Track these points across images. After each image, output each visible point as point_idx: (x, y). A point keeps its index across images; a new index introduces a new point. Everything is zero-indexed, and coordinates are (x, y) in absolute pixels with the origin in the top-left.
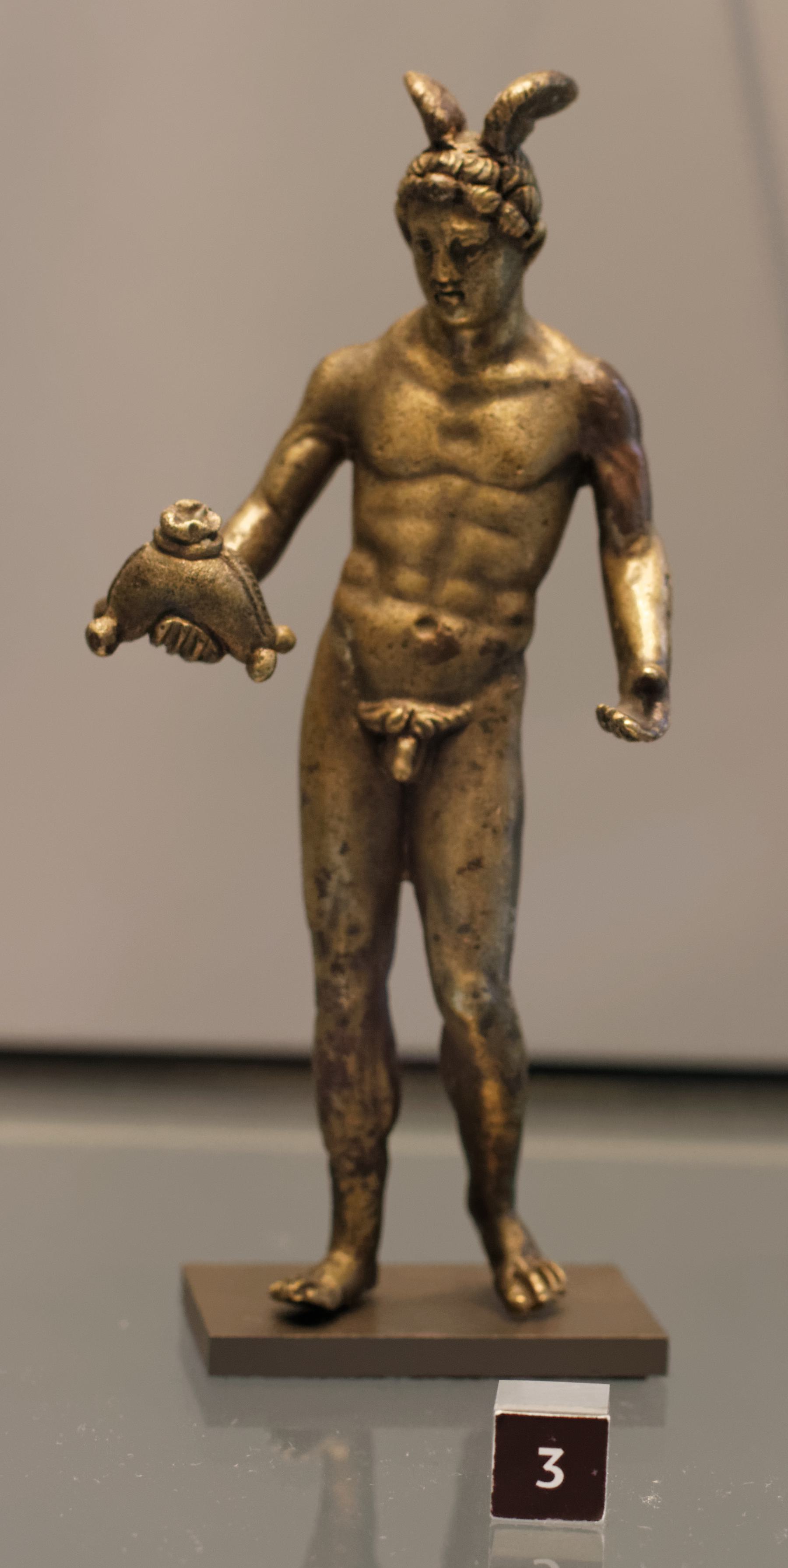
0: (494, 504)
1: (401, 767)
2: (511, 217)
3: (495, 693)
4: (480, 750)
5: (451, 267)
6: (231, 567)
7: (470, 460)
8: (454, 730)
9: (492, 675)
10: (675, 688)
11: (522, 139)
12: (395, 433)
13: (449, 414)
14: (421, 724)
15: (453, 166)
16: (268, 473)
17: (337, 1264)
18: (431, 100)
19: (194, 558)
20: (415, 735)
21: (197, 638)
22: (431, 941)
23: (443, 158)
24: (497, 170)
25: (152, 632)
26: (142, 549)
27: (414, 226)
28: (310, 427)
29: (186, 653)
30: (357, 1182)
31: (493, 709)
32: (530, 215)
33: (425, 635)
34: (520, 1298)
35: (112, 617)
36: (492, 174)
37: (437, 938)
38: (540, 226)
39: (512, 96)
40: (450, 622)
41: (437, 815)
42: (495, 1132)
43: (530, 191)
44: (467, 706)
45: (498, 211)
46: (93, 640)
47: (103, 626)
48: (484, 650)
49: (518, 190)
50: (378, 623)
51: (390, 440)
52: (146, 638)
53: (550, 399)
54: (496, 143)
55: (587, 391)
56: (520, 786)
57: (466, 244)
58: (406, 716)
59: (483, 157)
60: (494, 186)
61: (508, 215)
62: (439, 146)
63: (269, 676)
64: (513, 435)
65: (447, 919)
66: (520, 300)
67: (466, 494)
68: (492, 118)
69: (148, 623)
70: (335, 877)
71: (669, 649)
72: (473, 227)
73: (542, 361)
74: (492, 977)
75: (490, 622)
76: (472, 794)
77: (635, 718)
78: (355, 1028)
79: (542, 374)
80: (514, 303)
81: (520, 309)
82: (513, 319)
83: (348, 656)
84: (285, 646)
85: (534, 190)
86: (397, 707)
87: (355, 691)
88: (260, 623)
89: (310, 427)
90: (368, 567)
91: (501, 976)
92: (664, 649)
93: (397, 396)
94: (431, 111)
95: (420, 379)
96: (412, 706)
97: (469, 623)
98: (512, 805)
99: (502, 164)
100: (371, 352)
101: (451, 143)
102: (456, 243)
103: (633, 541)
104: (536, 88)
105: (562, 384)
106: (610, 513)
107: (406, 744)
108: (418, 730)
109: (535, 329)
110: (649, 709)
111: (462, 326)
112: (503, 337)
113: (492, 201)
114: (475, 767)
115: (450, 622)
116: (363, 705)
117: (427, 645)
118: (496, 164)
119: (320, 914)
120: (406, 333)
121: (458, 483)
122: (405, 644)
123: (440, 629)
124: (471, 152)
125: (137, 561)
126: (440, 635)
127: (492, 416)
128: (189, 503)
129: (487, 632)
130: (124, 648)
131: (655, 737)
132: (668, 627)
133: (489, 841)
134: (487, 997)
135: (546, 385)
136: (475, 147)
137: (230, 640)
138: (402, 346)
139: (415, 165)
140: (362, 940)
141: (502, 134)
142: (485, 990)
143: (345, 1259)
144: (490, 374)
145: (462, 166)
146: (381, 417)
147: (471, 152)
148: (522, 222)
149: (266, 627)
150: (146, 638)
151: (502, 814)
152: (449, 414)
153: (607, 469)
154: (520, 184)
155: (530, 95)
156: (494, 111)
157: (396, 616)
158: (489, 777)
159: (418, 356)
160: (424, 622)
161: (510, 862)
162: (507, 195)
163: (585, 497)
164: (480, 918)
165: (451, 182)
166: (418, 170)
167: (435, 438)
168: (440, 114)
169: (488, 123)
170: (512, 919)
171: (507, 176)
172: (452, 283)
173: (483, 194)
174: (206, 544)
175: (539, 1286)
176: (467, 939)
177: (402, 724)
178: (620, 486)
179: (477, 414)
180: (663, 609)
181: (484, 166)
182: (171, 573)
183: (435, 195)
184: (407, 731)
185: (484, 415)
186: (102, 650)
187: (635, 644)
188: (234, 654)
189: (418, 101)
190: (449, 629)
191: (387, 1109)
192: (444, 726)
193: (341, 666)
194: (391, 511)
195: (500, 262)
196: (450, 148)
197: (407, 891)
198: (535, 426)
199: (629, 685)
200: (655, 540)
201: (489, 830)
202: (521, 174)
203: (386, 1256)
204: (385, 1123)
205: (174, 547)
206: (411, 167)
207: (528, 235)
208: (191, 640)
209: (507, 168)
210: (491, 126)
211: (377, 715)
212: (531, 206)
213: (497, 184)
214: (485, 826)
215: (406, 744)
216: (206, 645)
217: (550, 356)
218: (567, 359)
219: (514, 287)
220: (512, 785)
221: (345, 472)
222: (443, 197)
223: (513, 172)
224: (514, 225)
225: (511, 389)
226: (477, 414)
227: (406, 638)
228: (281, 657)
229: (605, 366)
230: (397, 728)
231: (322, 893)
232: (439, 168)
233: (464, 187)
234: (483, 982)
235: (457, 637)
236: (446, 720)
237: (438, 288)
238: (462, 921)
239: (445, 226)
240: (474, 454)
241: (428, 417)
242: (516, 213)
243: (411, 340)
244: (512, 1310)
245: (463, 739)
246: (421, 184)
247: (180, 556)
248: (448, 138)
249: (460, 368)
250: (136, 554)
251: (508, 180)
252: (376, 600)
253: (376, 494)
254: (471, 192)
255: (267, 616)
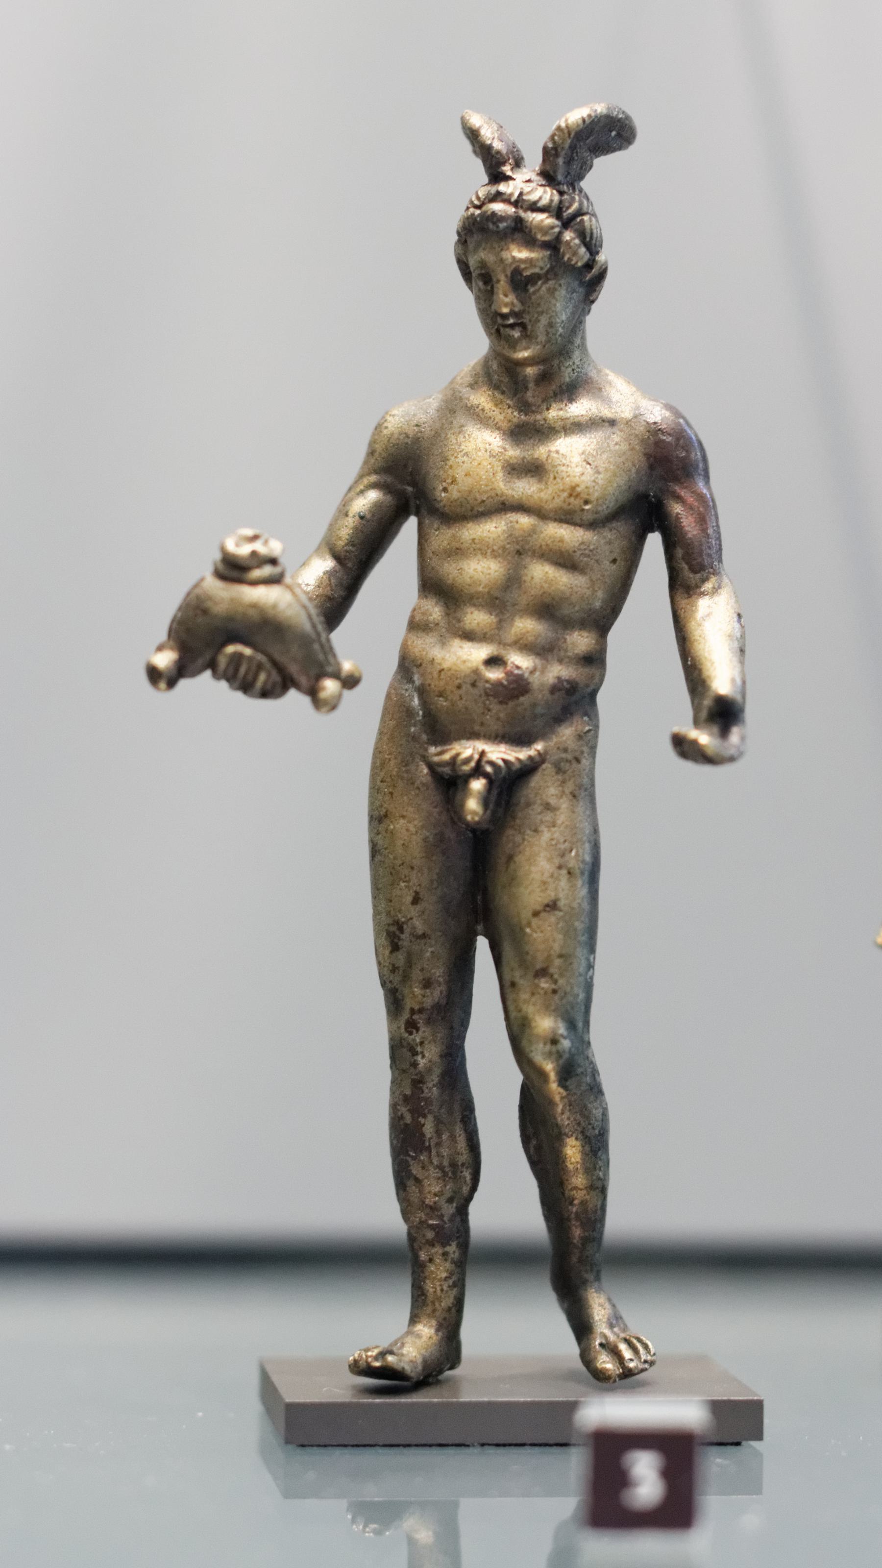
0: (561, 540)
1: (473, 805)
2: (572, 244)
3: (567, 733)
4: (552, 790)
5: (511, 298)
6: (293, 593)
7: (536, 497)
8: (528, 770)
9: (563, 715)
10: (750, 713)
11: (581, 177)
12: (459, 474)
13: (514, 453)
14: (492, 763)
15: (511, 195)
16: (332, 527)
17: (419, 1336)
18: (488, 134)
19: (254, 583)
20: (486, 775)
21: (260, 667)
22: (507, 989)
23: (502, 187)
24: (556, 198)
25: (212, 665)
26: (202, 579)
27: (473, 262)
28: (373, 478)
29: (246, 687)
30: (438, 1250)
31: (565, 750)
32: (591, 243)
33: (494, 675)
34: (606, 1363)
35: (172, 649)
36: (551, 201)
37: (513, 984)
38: (601, 258)
39: (570, 122)
40: (521, 661)
41: (510, 858)
42: (579, 1196)
43: (590, 219)
44: (539, 746)
45: (558, 237)
46: (154, 674)
47: (165, 660)
48: (554, 689)
49: (578, 219)
50: (445, 665)
51: (454, 481)
52: (208, 674)
53: (617, 436)
54: (555, 172)
55: (654, 430)
56: (596, 831)
57: (527, 273)
58: (476, 757)
59: (542, 185)
60: (554, 213)
61: (568, 243)
62: (496, 177)
63: (334, 708)
64: (579, 470)
65: (524, 962)
66: (583, 338)
67: (533, 531)
68: (550, 145)
69: (208, 656)
70: (407, 929)
71: (744, 683)
72: (533, 255)
73: (607, 401)
74: (571, 1025)
75: (560, 661)
76: (546, 835)
77: (713, 518)
78: (432, 1090)
79: (607, 413)
80: (578, 341)
81: (583, 347)
82: (576, 355)
83: (416, 701)
84: (350, 682)
85: (593, 219)
86: (466, 748)
87: (424, 737)
88: (325, 653)
89: (373, 478)
90: (435, 611)
91: (580, 1025)
92: (739, 681)
93: (461, 438)
94: (489, 142)
95: (482, 419)
96: (481, 745)
97: (538, 661)
98: (587, 846)
99: (561, 193)
100: (433, 403)
101: (509, 173)
102: (517, 272)
103: (704, 580)
104: (593, 114)
105: (628, 422)
106: (679, 552)
107: (478, 785)
108: (489, 769)
109: (599, 371)
110: (724, 733)
111: (524, 363)
112: (567, 376)
113: (553, 227)
114: (548, 807)
115: (521, 661)
116: (433, 750)
117: (498, 684)
118: (555, 192)
119: (394, 969)
120: (469, 379)
121: (525, 521)
122: (474, 685)
123: (509, 668)
124: (529, 181)
125: (198, 591)
126: (509, 674)
127: (557, 452)
128: (249, 532)
129: (557, 672)
130: (184, 684)
131: (732, 759)
132: (742, 662)
133: (564, 883)
134: (566, 1044)
135: (612, 423)
136: (534, 177)
137: (293, 669)
138: (465, 391)
139: (474, 198)
140: (436, 994)
141: (560, 161)
142: (565, 1038)
143: (426, 1331)
144: (554, 413)
145: (521, 194)
146: (445, 459)
147: (529, 181)
148: (583, 250)
149: (330, 657)
150: (208, 674)
151: (577, 855)
152: (514, 453)
153: (677, 509)
154: (580, 213)
155: (588, 121)
156: (552, 138)
157: (465, 657)
158: (562, 818)
159: (482, 399)
160: (493, 661)
161: (586, 906)
162: (566, 224)
163: (654, 542)
164: (557, 962)
165: (511, 210)
166: (476, 202)
167: (500, 475)
168: (497, 145)
169: (546, 151)
170: (590, 966)
171: (567, 204)
172: (513, 313)
173: (542, 221)
174: (267, 571)
175: (627, 1354)
176: (544, 984)
177: (473, 764)
178: (688, 524)
179: (541, 452)
180: (736, 645)
181: (545, 195)
182: (232, 600)
183: (494, 223)
184: (478, 771)
185: (550, 451)
186: (163, 685)
187: (709, 677)
188: (298, 687)
189: (473, 135)
190: (518, 667)
191: (467, 1175)
192: (517, 766)
193: (409, 713)
194: (457, 552)
195: (562, 292)
196: (508, 178)
197: (482, 944)
198: (602, 462)
199: (704, 714)
200: (726, 580)
201: (564, 872)
202: (581, 204)
203: (467, 1333)
204: (465, 1190)
205: (235, 574)
206: (472, 202)
207: (589, 266)
208: (254, 668)
209: (566, 197)
210: (549, 154)
211: (447, 757)
212: (592, 234)
213: (557, 211)
214: (560, 867)
215: (478, 785)
216: (269, 675)
217: (615, 396)
218: (632, 399)
219: (576, 326)
220: (588, 829)
221: (410, 526)
222: (502, 225)
223: (573, 200)
224: (575, 253)
225: (577, 427)
226: (541, 452)
227: (475, 679)
228: (346, 693)
229: (668, 407)
230: (466, 768)
231: (395, 948)
232: (498, 197)
233: (522, 214)
234: (562, 1030)
235: (526, 675)
236: (518, 759)
237: (499, 320)
238: (538, 966)
239: (505, 255)
240: (541, 490)
241: (492, 456)
242: (577, 241)
243: (473, 386)
244: (600, 1376)
245: (535, 781)
246: (479, 215)
247: (240, 581)
248: (507, 169)
249: (525, 407)
250: (196, 586)
251: (568, 208)
252: (443, 642)
253: (442, 537)
254: (531, 219)
255: (331, 648)
